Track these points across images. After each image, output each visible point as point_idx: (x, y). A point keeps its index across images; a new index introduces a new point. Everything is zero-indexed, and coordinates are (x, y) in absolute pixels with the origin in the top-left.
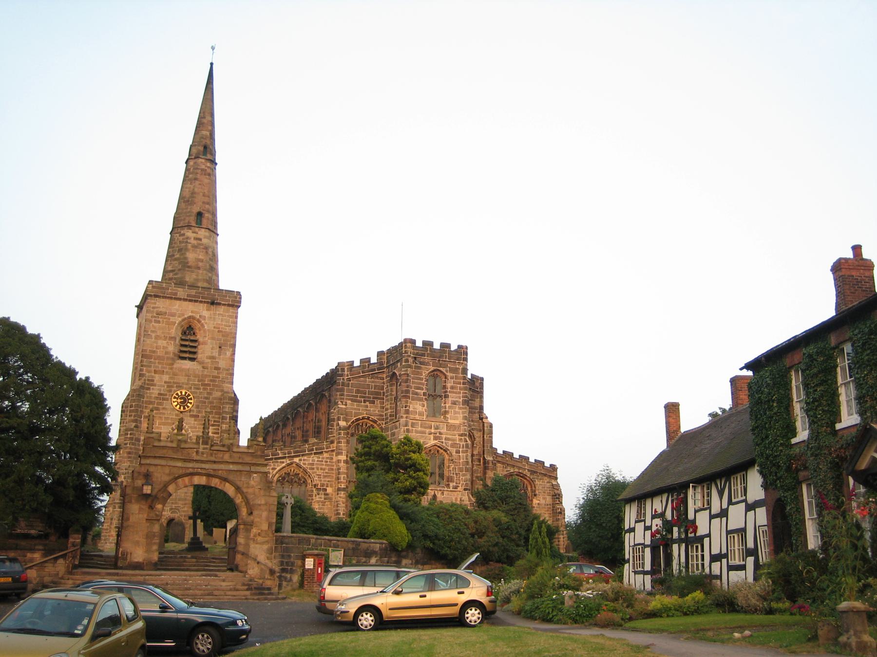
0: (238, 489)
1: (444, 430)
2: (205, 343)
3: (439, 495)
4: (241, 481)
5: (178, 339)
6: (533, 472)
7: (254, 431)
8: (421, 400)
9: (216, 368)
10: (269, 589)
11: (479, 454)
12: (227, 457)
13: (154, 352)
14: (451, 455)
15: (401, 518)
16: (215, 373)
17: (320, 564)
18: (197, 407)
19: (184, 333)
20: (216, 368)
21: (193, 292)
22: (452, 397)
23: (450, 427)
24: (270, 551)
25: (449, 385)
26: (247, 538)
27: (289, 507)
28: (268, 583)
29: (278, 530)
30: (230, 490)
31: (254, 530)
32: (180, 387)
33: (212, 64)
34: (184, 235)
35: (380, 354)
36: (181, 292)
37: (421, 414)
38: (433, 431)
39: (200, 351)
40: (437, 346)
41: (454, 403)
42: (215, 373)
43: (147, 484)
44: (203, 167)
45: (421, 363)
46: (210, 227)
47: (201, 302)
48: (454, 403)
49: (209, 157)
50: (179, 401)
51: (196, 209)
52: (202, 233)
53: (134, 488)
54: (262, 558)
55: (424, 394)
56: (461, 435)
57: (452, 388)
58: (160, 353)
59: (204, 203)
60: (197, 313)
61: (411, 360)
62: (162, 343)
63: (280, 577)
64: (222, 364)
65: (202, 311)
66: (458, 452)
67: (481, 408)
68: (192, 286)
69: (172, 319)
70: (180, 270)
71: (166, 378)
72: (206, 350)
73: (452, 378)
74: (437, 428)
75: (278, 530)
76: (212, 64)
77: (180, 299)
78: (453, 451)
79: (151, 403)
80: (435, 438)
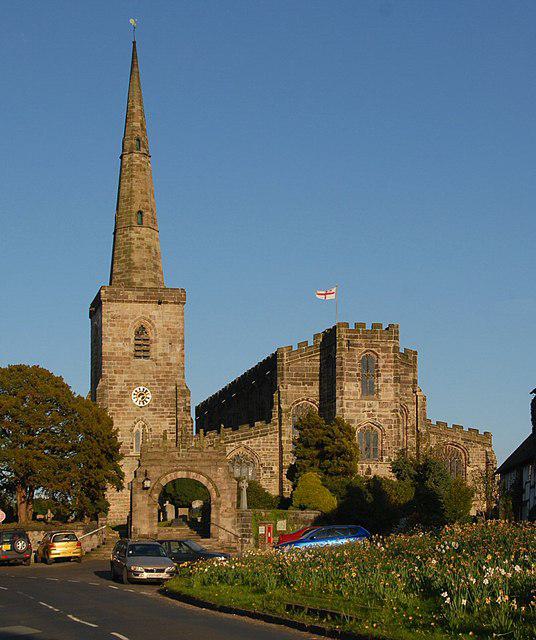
0: (209, 479)
1: (377, 408)
2: (156, 341)
3: (373, 469)
4: (211, 473)
5: (132, 342)
6: (466, 441)
7: (197, 408)
8: (355, 381)
9: (168, 364)
10: (235, 548)
11: (412, 426)
12: (199, 456)
13: (113, 353)
14: (383, 430)
15: (101, 577)
16: (168, 369)
17: (269, 531)
18: (155, 401)
19: (137, 333)
20: (168, 364)
21: (142, 294)
22: (384, 375)
23: (383, 405)
24: (234, 523)
25: (381, 364)
26: (217, 514)
27: (245, 490)
28: (233, 545)
29: (239, 506)
30: (203, 480)
31: (222, 508)
32: (138, 385)
33: (134, 43)
34: (127, 236)
35: (316, 336)
36: (131, 295)
37: (355, 394)
38: (366, 409)
39: (152, 350)
40: (369, 327)
41: (386, 381)
42: (168, 369)
43: (147, 479)
44: (138, 162)
45: (354, 345)
46: (151, 225)
47: (150, 302)
48: (386, 381)
49: (143, 150)
50: (140, 399)
51: (136, 208)
52: (144, 231)
53: (138, 483)
54: (228, 528)
55: (358, 375)
56: (394, 411)
57: (384, 366)
58: (118, 354)
59: (142, 200)
60: (147, 313)
61: (345, 343)
62: (119, 344)
63: (241, 541)
64: (173, 360)
65: (151, 309)
66: (390, 427)
67: (415, 382)
68: (140, 289)
69: (126, 321)
70: (127, 272)
71: (125, 376)
72: (158, 348)
73: (383, 357)
74: (370, 406)
75: (239, 506)
76: (134, 43)
77: (131, 302)
78: (386, 427)
79: (114, 401)
80: (369, 416)
